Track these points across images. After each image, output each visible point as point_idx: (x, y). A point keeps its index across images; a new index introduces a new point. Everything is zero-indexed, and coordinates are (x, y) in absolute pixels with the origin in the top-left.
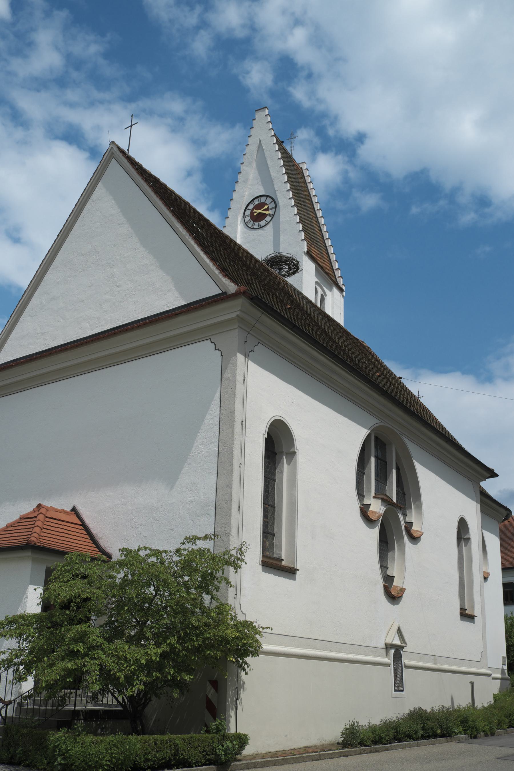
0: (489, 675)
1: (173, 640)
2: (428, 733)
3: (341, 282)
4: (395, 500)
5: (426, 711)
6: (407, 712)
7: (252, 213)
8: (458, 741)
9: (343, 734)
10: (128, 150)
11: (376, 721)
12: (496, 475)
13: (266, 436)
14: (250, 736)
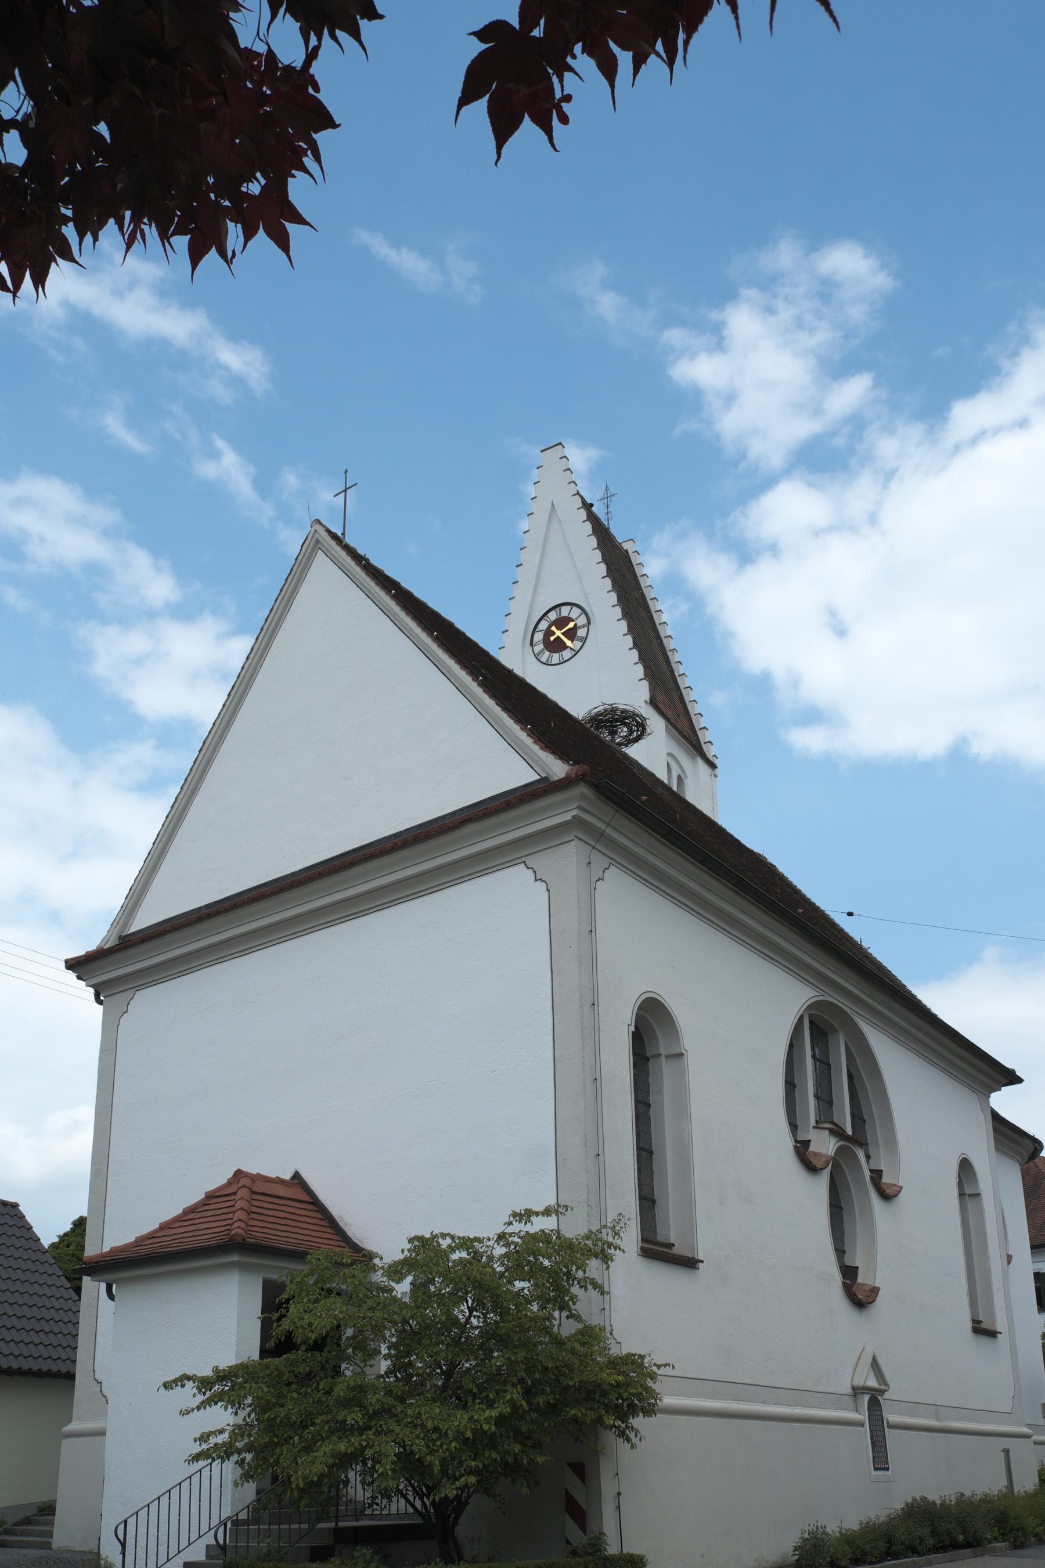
0: (1029, 1436)
1: (514, 1394)
2: (942, 1541)
4: (849, 1132)
5: (934, 1503)
6: (899, 1505)
7: (549, 633)
8: (993, 1552)
9: (796, 1549)
10: (343, 534)
11: (852, 1524)
12: (1019, 1080)
13: (633, 1028)
14: (648, 1557)
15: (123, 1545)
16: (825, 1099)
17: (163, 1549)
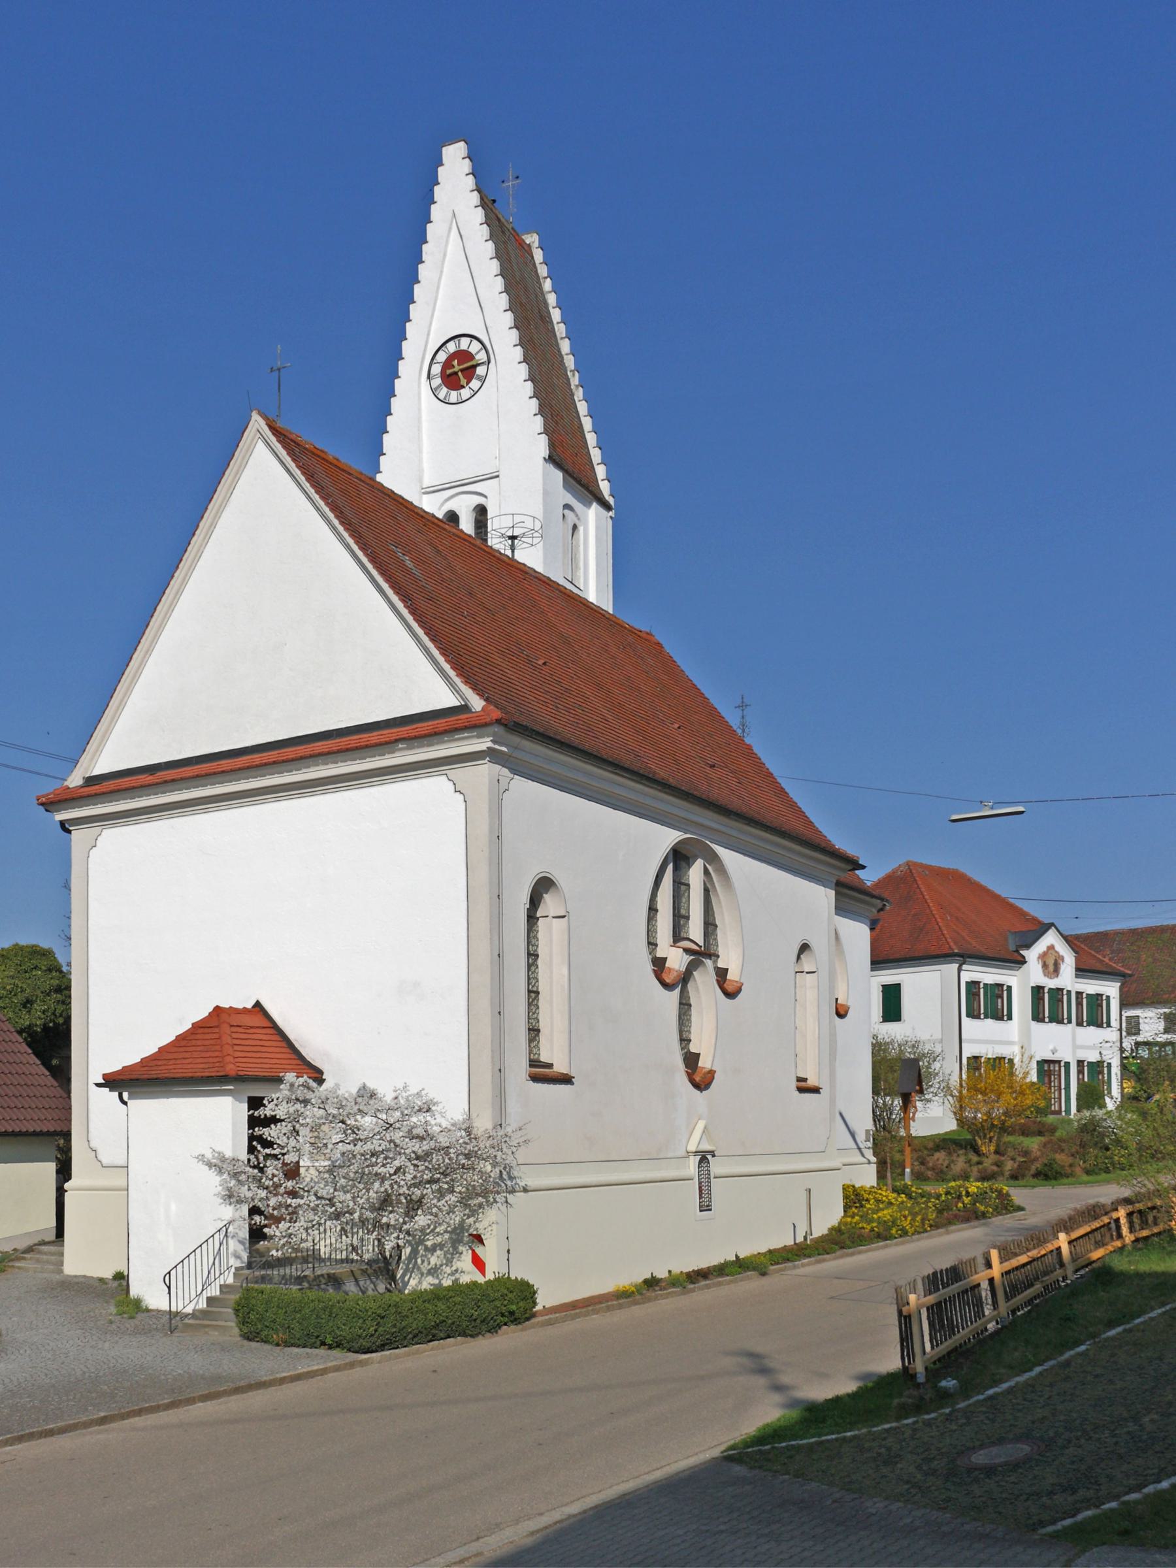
3: (605, 487)
15: (169, 1288)
16: (680, 919)
17: (187, 1296)
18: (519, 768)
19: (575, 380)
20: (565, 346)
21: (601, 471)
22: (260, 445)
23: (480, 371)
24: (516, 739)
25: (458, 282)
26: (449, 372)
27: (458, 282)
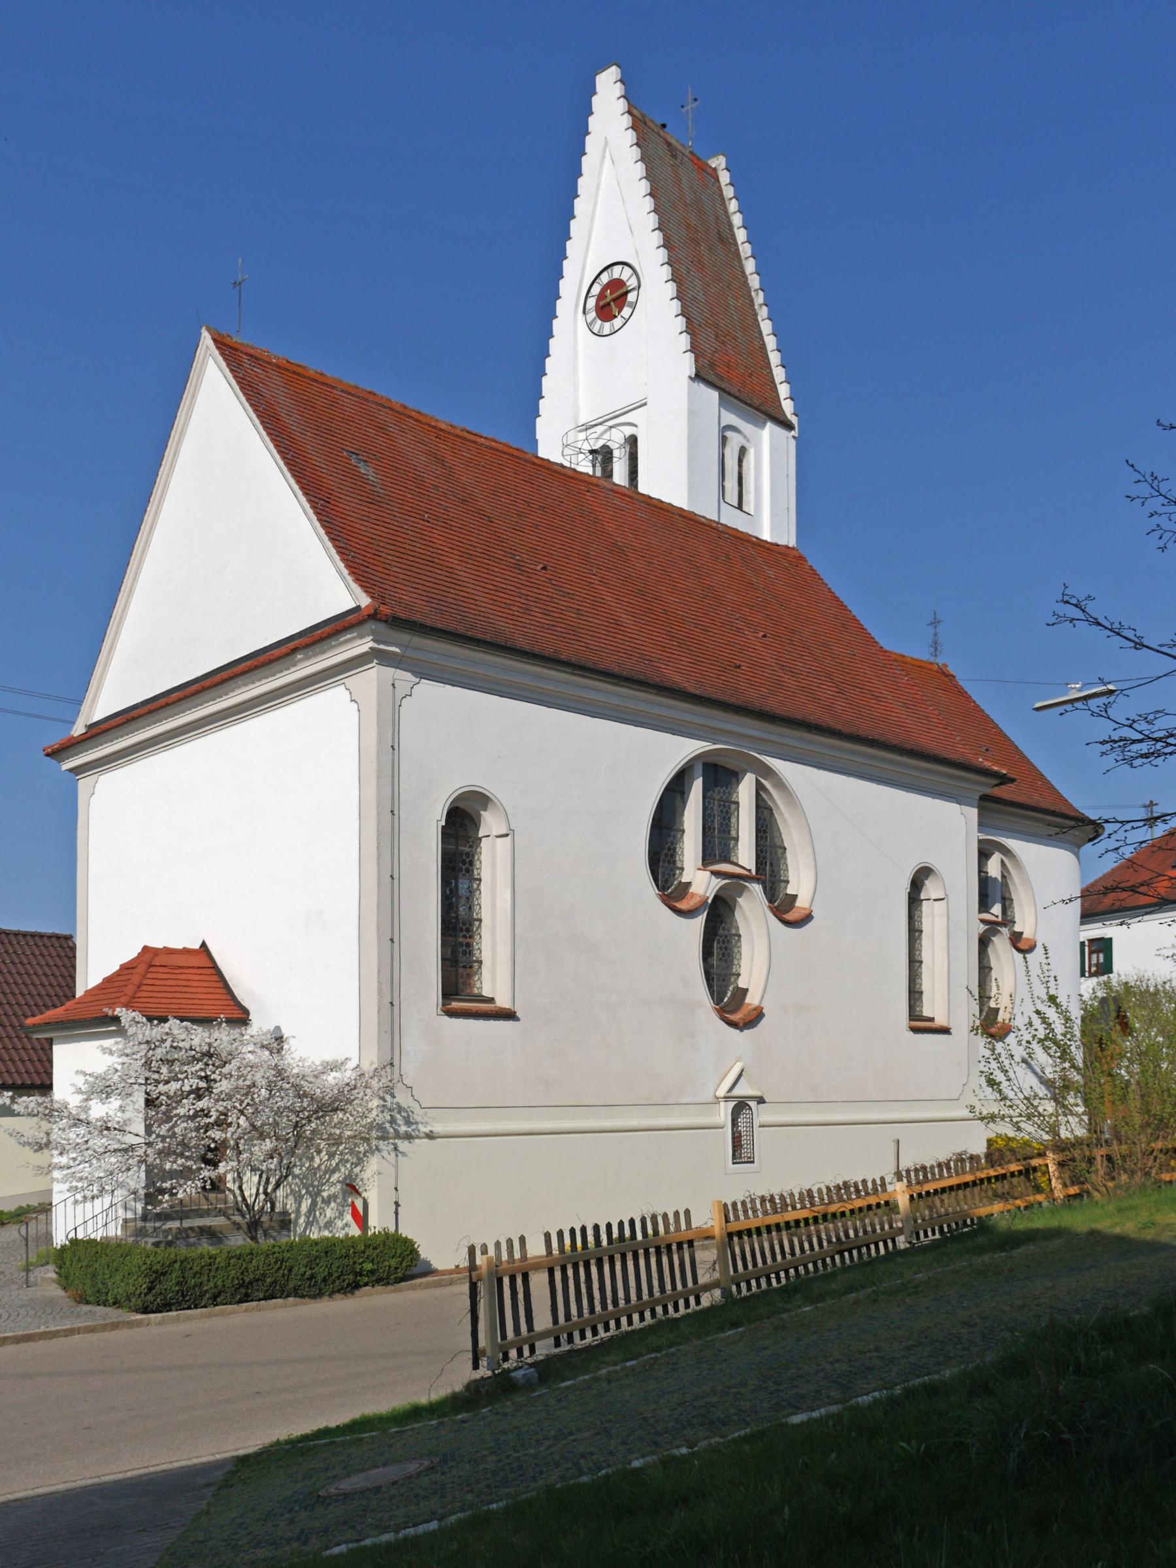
3: (788, 407)
18: (425, 672)
19: (759, 298)
20: (750, 266)
21: (784, 390)
22: (211, 361)
23: (631, 297)
24: (405, 637)
25: (613, 212)
26: (602, 303)
27: (613, 212)
